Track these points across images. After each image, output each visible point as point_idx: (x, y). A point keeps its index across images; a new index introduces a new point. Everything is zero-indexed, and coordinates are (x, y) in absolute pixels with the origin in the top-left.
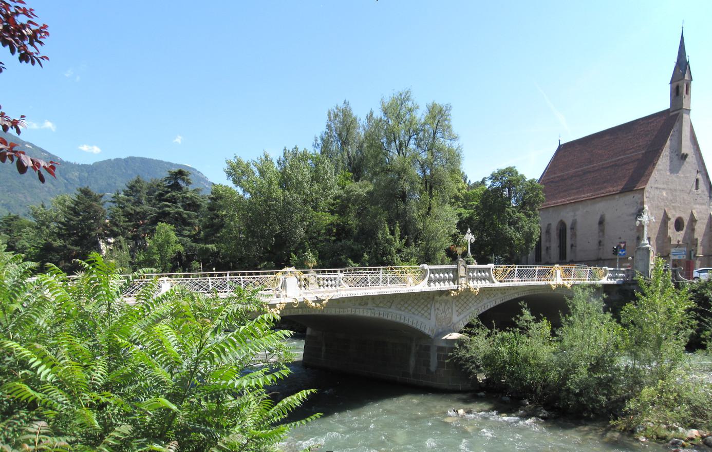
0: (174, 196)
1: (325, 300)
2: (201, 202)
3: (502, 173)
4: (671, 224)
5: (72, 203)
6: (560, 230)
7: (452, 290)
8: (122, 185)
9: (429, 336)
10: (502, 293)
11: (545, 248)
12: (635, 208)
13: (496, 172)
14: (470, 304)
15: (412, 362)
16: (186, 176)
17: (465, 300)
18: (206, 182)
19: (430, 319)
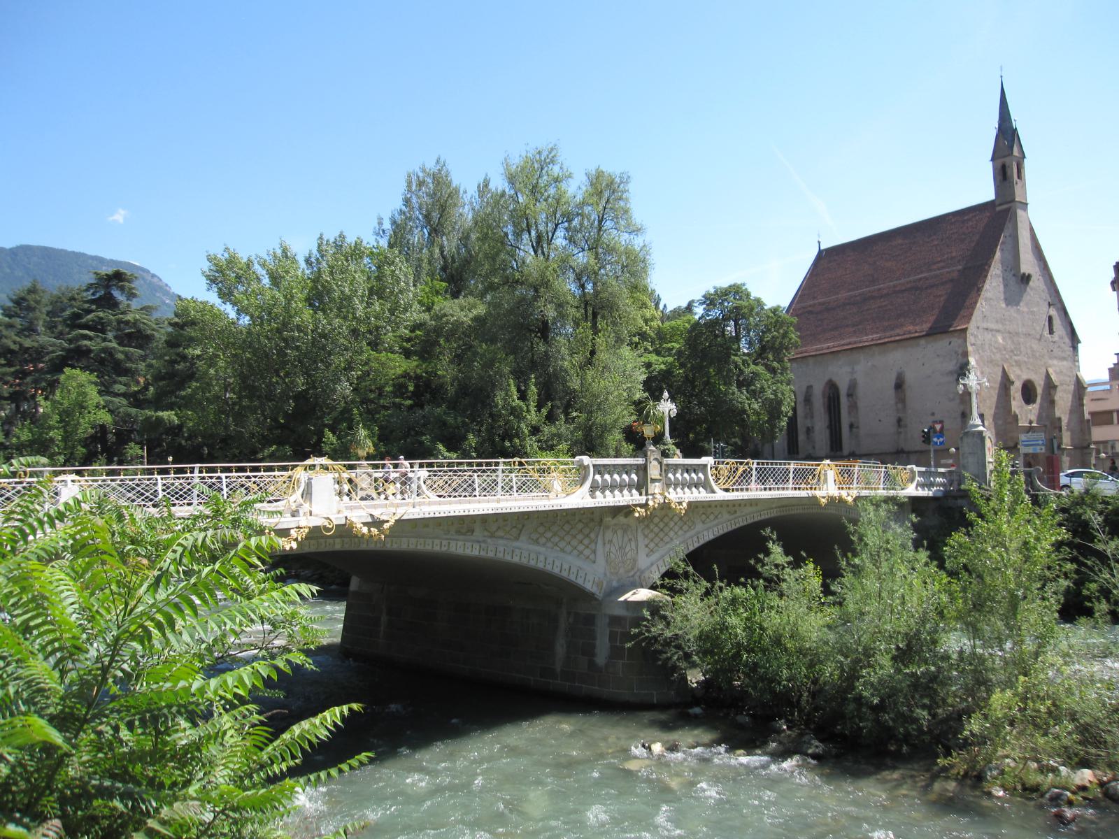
1: (387, 521)
2: (153, 330)
3: (723, 294)
6: (829, 398)
7: (636, 505)
9: (593, 594)
11: (804, 429)
12: (955, 362)
13: (712, 291)
15: (560, 649)
19: (594, 562)
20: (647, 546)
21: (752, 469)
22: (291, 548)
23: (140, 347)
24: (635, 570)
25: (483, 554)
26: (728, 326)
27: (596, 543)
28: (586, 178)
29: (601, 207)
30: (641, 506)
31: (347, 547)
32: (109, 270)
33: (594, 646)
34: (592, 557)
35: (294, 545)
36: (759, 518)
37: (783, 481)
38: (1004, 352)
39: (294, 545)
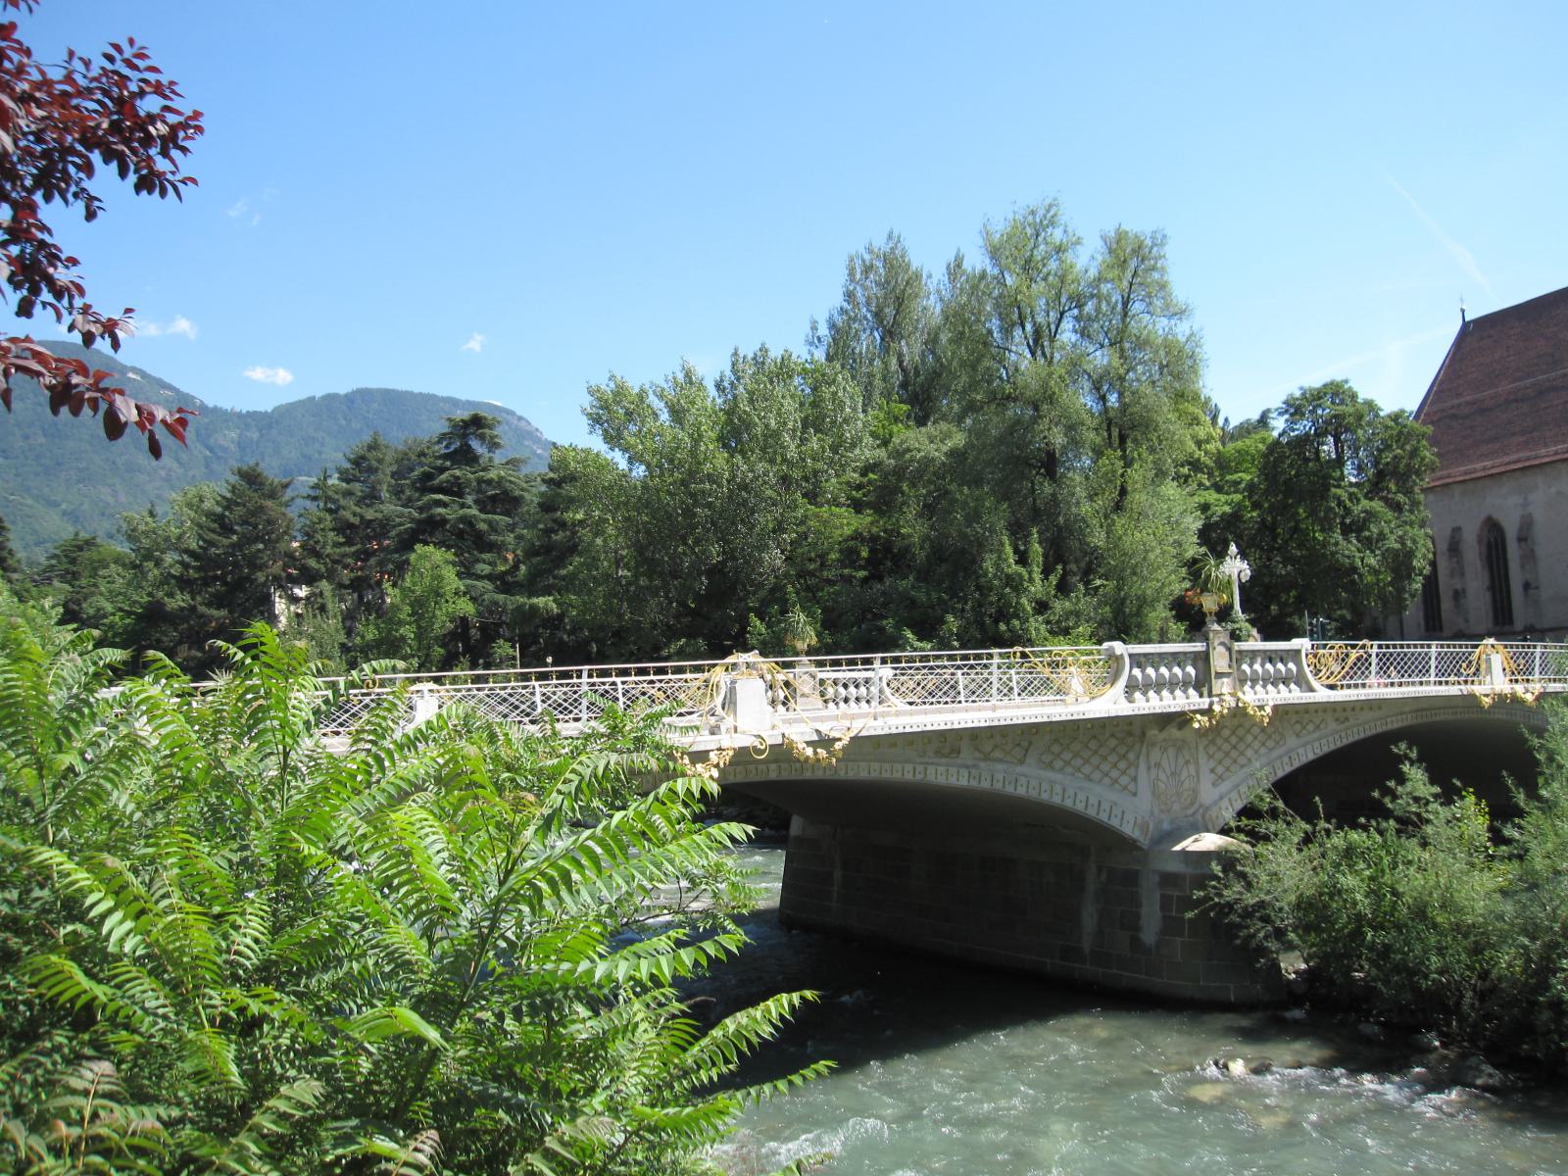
1: (840, 739)
3: (1315, 397)
5: (218, 503)
6: (1489, 546)
7: (1195, 712)
8: (336, 455)
9: (1135, 841)
11: (1451, 593)
14: (1249, 753)
15: (1089, 918)
17: (1234, 740)
19: (1135, 794)
20: (1212, 771)
23: (507, 513)
24: (1196, 806)
25: (974, 783)
26: (1323, 444)
27: (1137, 767)
29: (1125, 284)
30: (1202, 712)
32: (466, 415)
33: (1138, 917)
34: (1131, 787)
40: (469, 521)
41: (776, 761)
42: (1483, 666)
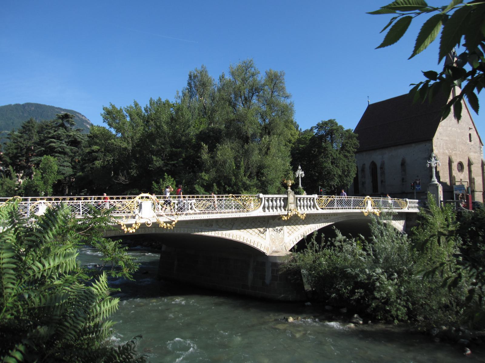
0: (60, 134)
1: (174, 221)
2: (82, 139)
3: (325, 123)
4: (455, 166)
7: (283, 215)
8: (19, 123)
9: (264, 253)
10: (325, 218)
13: (321, 122)
15: (250, 276)
16: (71, 118)
18: (88, 123)
19: (265, 239)
20: (288, 233)
21: (334, 200)
22: (133, 232)
23: (76, 147)
26: (327, 138)
28: (265, 74)
29: (272, 86)
30: (286, 215)
31: (157, 232)
32: (63, 113)
35: (134, 231)
36: (338, 221)
37: (348, 205)
38: (449, 150)
39: (134, 231)
40: (63, 148)
41: (155, 227)
42: (366, 204)
